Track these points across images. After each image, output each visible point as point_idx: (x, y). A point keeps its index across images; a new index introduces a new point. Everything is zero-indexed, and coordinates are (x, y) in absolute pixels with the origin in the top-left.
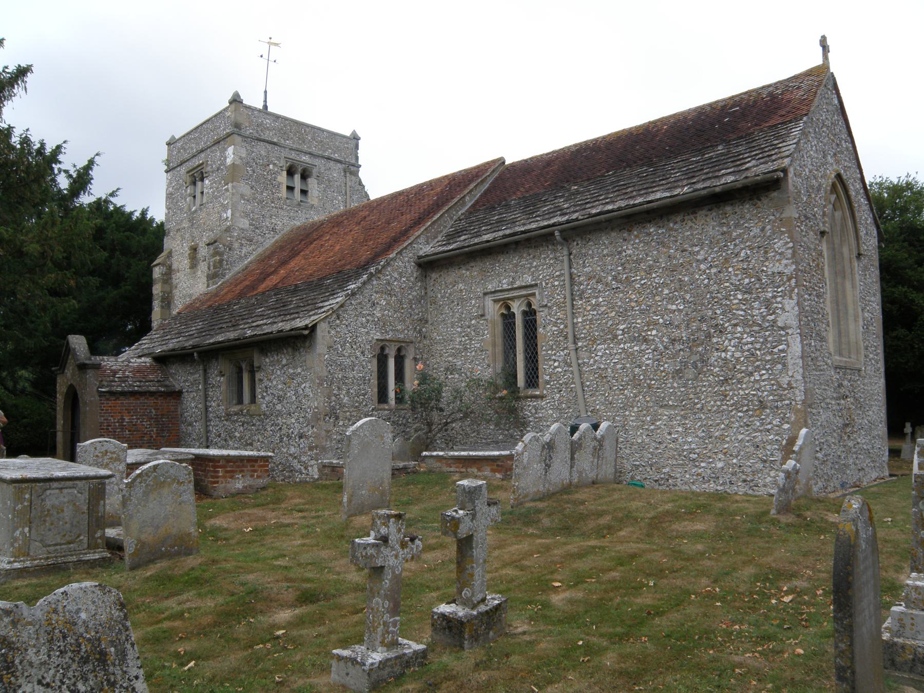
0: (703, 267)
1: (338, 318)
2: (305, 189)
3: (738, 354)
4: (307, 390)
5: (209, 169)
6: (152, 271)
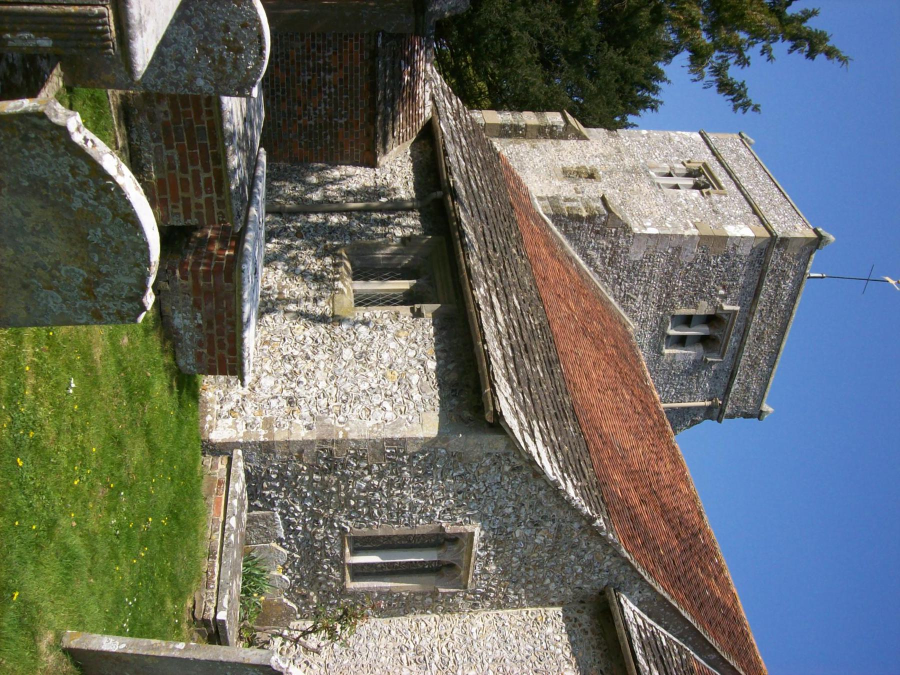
1: (513, 469)
2: (688, 341)
4: (378, 415)
5: (715, 197)
6: (556, 110)
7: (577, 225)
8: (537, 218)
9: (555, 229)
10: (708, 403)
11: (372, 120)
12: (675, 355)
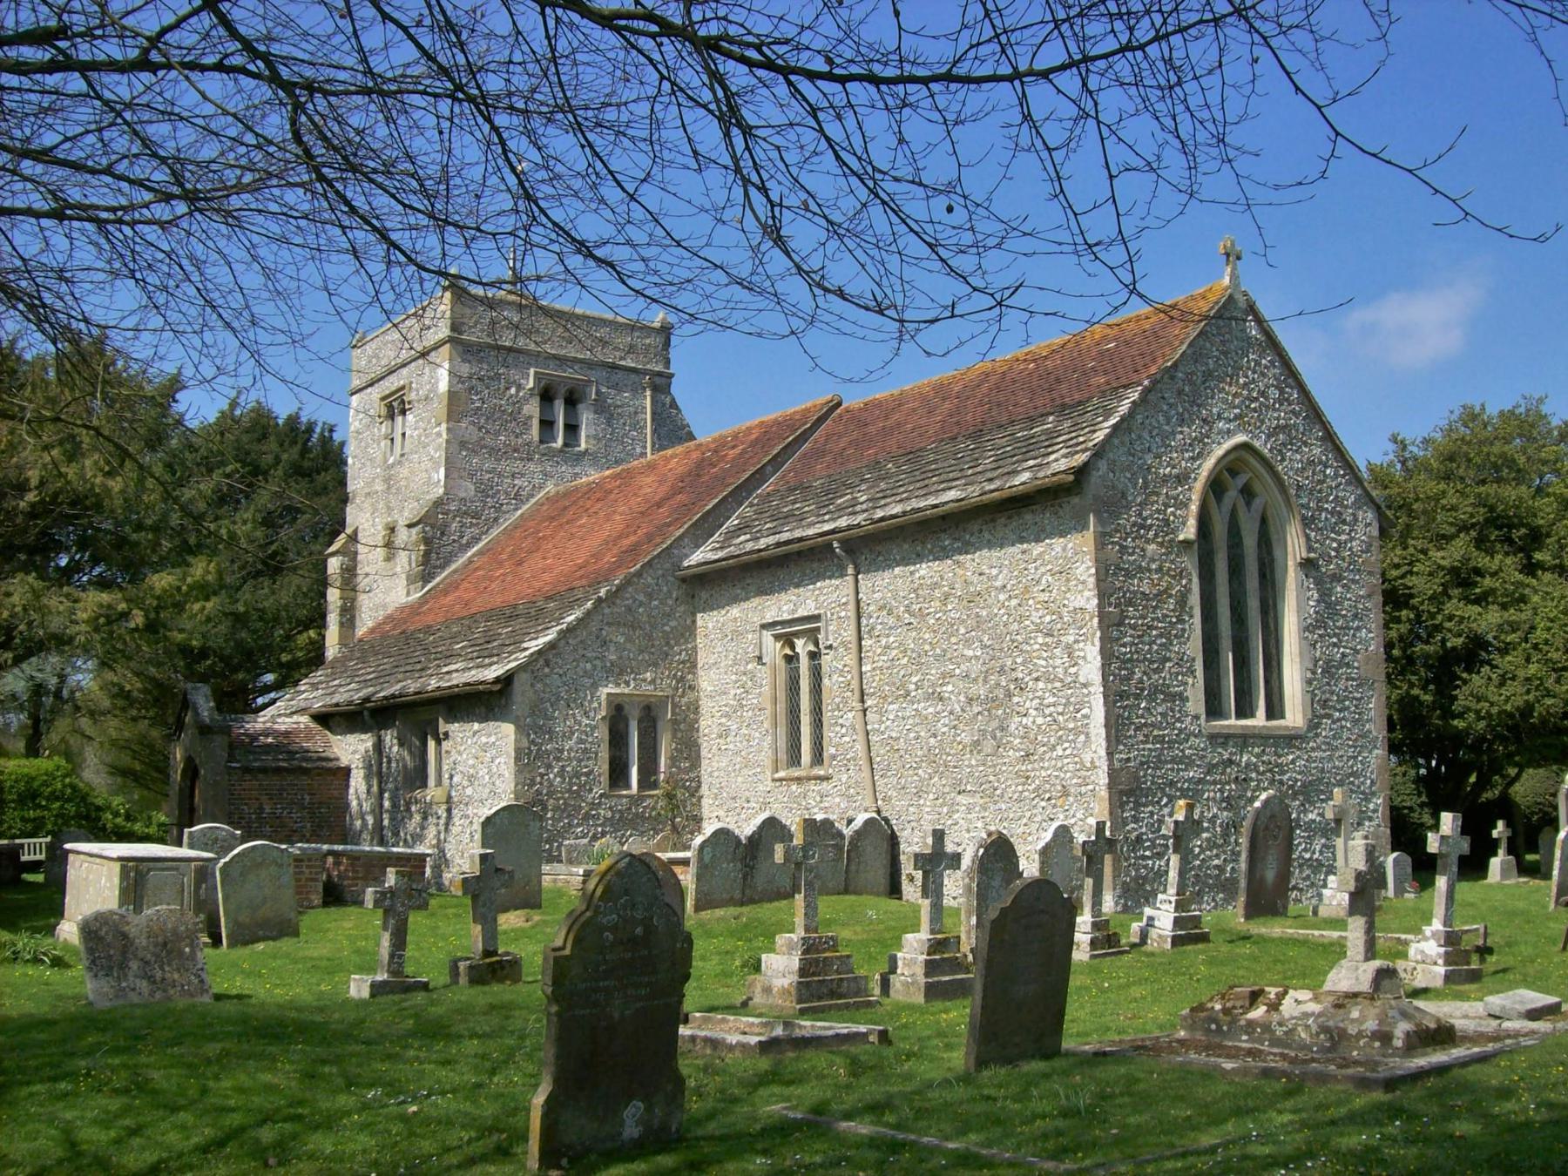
0: (1002, 597)
3: (1040, 721)
4: (503, 767)
7: (434, 556)
8: (423, 600)
9: (438, 579)
10: (648, 393)
11: (305, 771)
12: (587, 436)
